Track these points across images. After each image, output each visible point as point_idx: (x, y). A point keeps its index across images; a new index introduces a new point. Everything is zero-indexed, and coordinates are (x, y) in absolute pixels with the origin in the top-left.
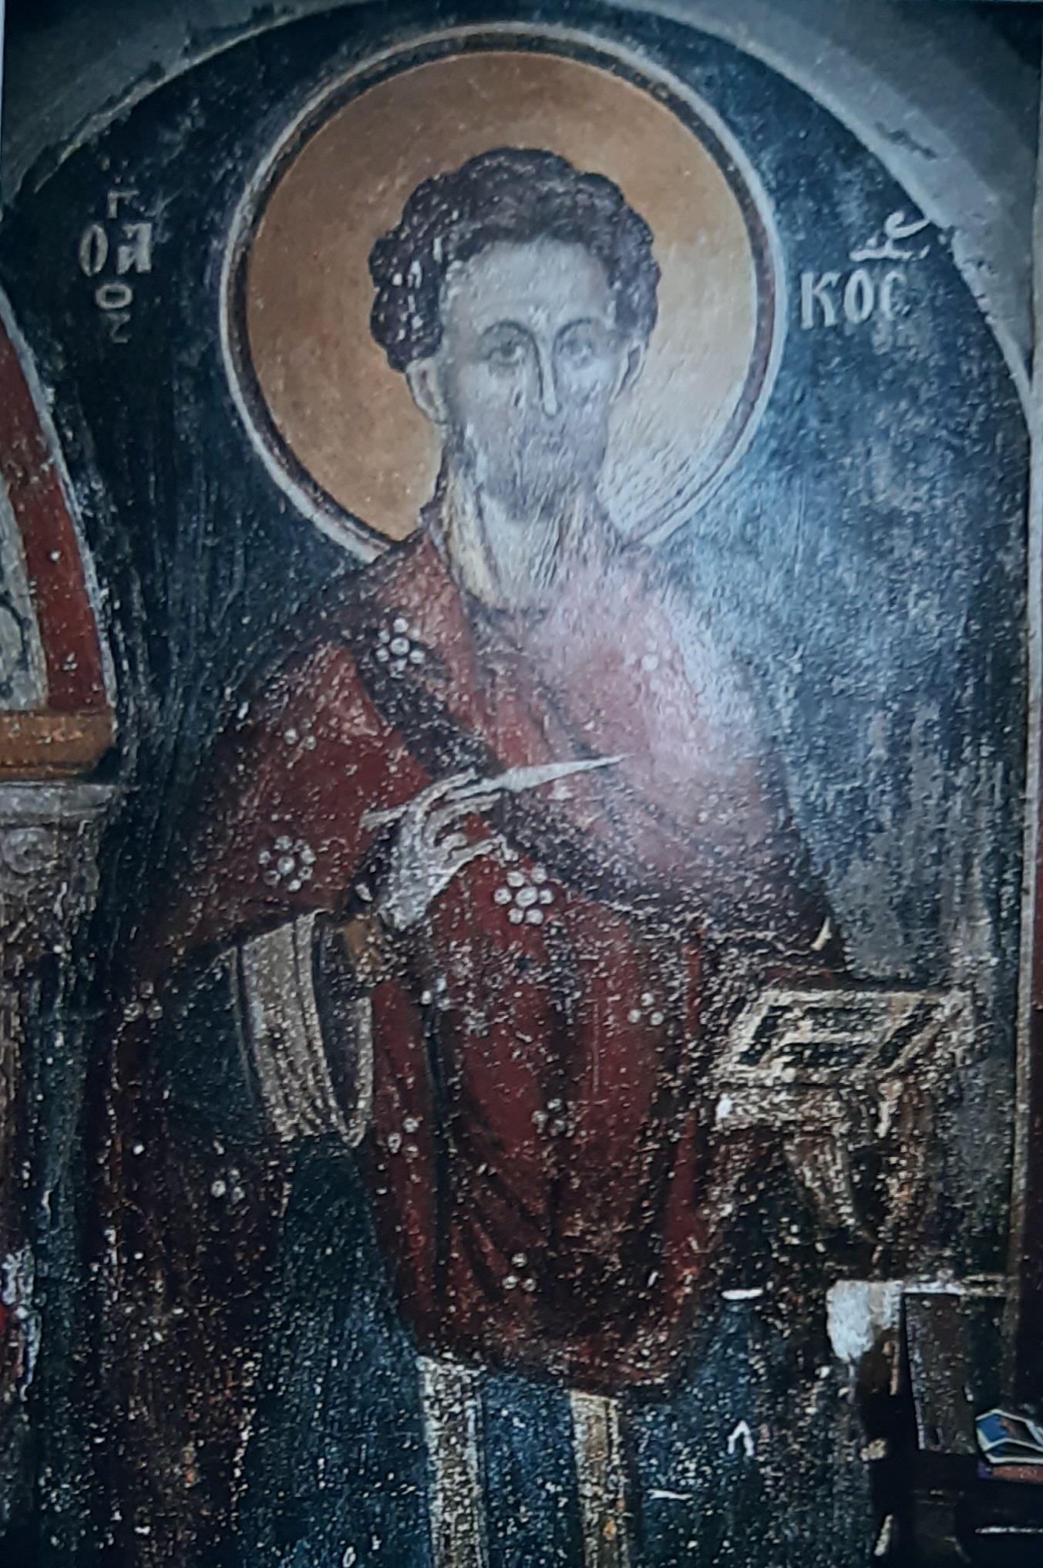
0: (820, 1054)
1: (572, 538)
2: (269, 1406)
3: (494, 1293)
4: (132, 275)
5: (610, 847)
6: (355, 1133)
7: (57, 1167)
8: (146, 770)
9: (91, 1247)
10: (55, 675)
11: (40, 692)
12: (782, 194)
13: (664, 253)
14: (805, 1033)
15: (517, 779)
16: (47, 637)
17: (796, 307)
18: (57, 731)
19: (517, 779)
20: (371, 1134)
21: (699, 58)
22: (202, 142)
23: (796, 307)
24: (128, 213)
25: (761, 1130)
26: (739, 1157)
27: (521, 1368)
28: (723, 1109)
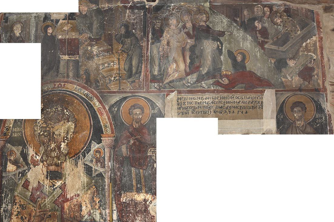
0: (154, 151)
1: (102, 114)
2: (123, 170)
3: (136, 164)
4: (116, 111)
5: (145, 169)
6: (128, 156)
7: (112, 158)
8: (116, 137)
9: (114, 162)
10: (112, 132)
11: (111, 133)
12: (151, 106)
13: (145, 109)
14: (153, 150)
15: (137, 137)
16: (111, 130)
17: (152, 112)
18: (112, 135)
19: (137, 137)
20: (129, 156)
21: (146, 99)
22: (119, 104)
23: (152, 112)
24: (115, 107)
25: (150, 155)
26: (149, 157)
27: (137, 168)
28: (148, 154)
